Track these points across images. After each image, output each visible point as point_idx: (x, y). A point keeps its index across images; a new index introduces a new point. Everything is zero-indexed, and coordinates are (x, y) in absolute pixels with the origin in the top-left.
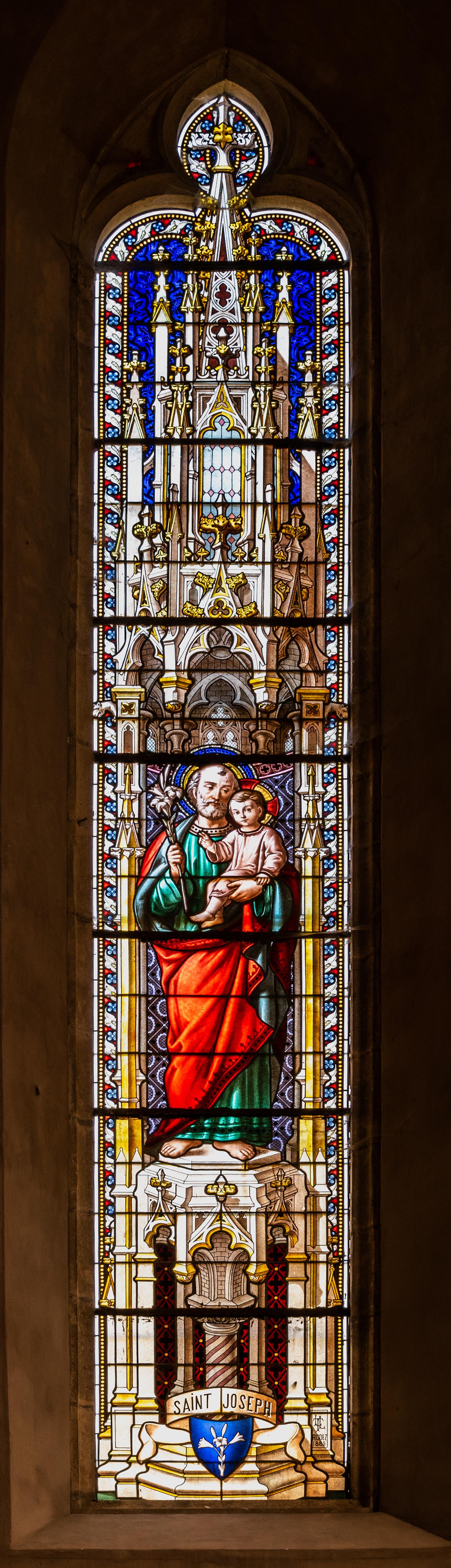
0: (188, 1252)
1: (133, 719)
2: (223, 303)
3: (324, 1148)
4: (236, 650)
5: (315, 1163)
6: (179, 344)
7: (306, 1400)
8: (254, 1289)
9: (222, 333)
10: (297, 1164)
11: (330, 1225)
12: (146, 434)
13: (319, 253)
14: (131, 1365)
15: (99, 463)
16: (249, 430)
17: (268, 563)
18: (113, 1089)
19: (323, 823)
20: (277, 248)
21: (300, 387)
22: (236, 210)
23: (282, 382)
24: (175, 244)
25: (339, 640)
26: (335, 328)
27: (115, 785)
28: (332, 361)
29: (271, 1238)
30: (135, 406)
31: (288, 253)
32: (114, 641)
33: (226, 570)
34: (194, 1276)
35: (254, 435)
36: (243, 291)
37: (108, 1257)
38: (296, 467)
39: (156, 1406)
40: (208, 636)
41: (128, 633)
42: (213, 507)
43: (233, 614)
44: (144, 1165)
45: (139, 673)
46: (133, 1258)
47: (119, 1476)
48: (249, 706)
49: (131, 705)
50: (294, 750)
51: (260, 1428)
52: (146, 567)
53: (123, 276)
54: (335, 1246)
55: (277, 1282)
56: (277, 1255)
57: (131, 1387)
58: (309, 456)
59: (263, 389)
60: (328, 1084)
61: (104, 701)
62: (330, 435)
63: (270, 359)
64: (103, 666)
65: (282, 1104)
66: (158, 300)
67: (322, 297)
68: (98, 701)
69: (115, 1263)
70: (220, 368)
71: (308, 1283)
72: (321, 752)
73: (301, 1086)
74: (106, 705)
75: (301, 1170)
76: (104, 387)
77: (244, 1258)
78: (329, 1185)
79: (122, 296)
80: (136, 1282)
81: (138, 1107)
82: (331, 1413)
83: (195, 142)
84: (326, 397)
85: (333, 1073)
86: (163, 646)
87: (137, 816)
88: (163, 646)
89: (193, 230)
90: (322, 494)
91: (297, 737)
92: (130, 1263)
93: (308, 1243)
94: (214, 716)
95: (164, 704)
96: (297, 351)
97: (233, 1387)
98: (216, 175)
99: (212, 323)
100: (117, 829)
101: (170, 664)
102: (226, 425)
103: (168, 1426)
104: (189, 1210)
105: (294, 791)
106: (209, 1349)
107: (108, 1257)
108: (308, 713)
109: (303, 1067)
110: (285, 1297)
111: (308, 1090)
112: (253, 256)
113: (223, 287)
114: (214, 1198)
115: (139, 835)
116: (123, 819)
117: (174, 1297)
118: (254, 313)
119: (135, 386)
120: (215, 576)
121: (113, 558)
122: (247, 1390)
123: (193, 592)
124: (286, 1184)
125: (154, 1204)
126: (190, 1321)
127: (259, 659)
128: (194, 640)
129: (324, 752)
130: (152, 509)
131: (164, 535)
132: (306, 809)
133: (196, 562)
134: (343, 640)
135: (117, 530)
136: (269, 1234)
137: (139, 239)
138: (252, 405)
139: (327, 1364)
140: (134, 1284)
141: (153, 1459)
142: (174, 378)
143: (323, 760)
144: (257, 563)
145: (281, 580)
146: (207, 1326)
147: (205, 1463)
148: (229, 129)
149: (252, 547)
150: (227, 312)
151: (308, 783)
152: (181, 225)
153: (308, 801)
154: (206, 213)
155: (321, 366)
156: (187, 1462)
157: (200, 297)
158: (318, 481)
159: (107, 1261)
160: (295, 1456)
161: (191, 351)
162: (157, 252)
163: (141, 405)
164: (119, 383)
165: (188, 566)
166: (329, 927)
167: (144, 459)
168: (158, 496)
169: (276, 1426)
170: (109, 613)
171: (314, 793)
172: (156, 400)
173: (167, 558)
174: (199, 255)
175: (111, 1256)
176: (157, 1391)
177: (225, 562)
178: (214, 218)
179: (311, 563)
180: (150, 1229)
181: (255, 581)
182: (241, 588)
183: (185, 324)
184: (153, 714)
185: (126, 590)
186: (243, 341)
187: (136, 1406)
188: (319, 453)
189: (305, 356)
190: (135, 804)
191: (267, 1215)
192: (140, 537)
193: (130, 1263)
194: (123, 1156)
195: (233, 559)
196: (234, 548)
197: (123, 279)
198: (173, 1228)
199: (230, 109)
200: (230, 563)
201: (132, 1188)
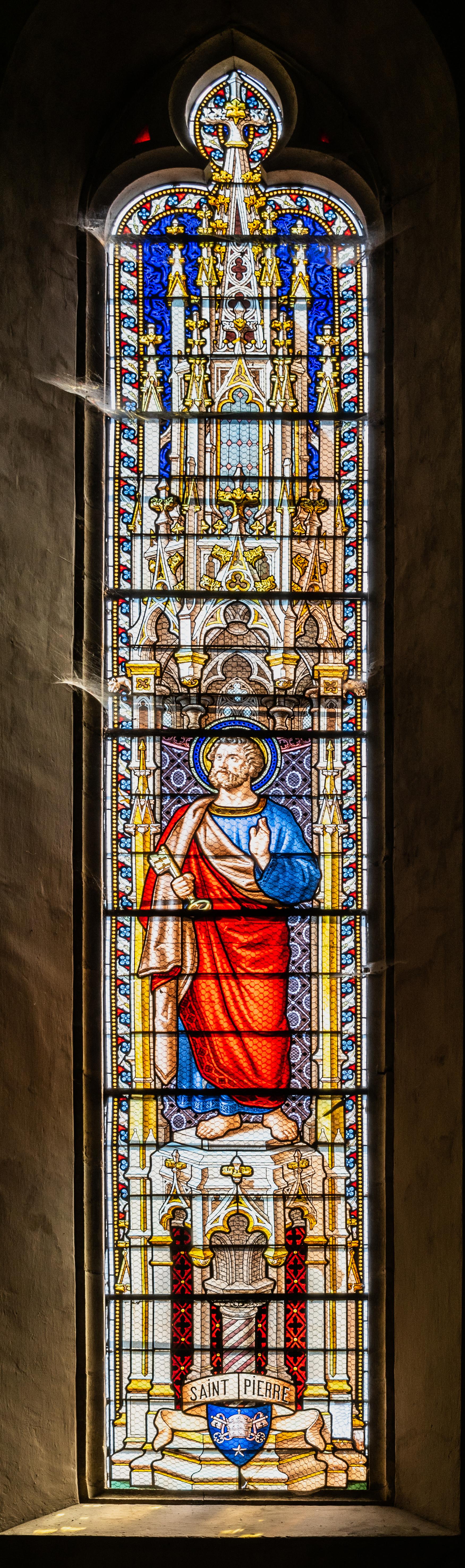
1: (148, 695)
3: (343, 1130)
6: (195, 318)
7: (326, 1387)
8: (272, 1273)
11: (348, 1207)
14: (147, 1351)
15: (116, 435)
16: (268, 403)
23: (300, 356)
24: (190, 218)
25: (357, 584)
27: (128, 761)
28: (350, 335)
29: (289, 1221)
31: (303, 226)
32: (128, 614)
33: (243, 543)
35: (273, 408)
37: (123, 1240)
38: (315, 442)
39: (172, 1392)
40: (225, 612)
41: (143, 607)
43: (250, 588)
48: (266, 682)
50: (312, 727)
51: (279, 1414)
53: (137, 249)
55: (296, 1267)
56: (296, 1241)
60: (346, 1065)
61: (118, 676)
62: (350, 408)
63: (288, 333)
68: (113, 676)
70: (237, 342)
71: (328, 1267)
72: (340, 729)
73: (318, 1066)
74: (121, 680)
75: (319, 1152)
76: (121, 360)
78: (348, 1168)
79: (137, 270)
80: (153, 1266)
81: (153, 1087)
84: (344, 371)
85: (351, 1055)
86: (179, 620)
87: (152, 793)
88: (179, 620)
89: (207, 204)
90: (341, 469)
94: (230, 692)
95: (179, 679)
96: (315, 330)
97: (251, 1373)
98: (229, 150)
101: (186, 640)
103: (185, 1412)
105: (311, 767)
106: (226, 1333)
107: (123, 1240)
109: (321, 1047)
110: (304, 1281)
111: (326, 1071)
112: (270, 230)
117: (191, 1282)
118: (271, 287)
122: (265, 1375)
123: (210, 565)
124: (304, 1165)
126: (208, 1305)
127: (276, 635)
128: (209, 617)
129: (342, 728)
131: (181, 508)
132: (326, 784)
134: (362, 553)
137: (153, 213)
138: (271, 378)
140: (149, 1267)
141: (171, 1446)
143: (342, 734)
145: (299, 554)
147: (222, 1452)
152: (195, 199)
153: (327, 777)
155: (340, 340)
156: (204, 1449)
164: (137, 357)
168: (175, 468)
169: (295, 1412)
170: (125, 586)
174: (213, 229)
175: (126, 1239)
176: (173, 1377)
177: (243, 537)
179: (330, 537)
188: (338, 427)
189: (323, 330)
190: (151, 779)
195: (251, 531)
197: (138, 252)
198: (189, 1210)
199: (242, 85)
201: (147, 1170)
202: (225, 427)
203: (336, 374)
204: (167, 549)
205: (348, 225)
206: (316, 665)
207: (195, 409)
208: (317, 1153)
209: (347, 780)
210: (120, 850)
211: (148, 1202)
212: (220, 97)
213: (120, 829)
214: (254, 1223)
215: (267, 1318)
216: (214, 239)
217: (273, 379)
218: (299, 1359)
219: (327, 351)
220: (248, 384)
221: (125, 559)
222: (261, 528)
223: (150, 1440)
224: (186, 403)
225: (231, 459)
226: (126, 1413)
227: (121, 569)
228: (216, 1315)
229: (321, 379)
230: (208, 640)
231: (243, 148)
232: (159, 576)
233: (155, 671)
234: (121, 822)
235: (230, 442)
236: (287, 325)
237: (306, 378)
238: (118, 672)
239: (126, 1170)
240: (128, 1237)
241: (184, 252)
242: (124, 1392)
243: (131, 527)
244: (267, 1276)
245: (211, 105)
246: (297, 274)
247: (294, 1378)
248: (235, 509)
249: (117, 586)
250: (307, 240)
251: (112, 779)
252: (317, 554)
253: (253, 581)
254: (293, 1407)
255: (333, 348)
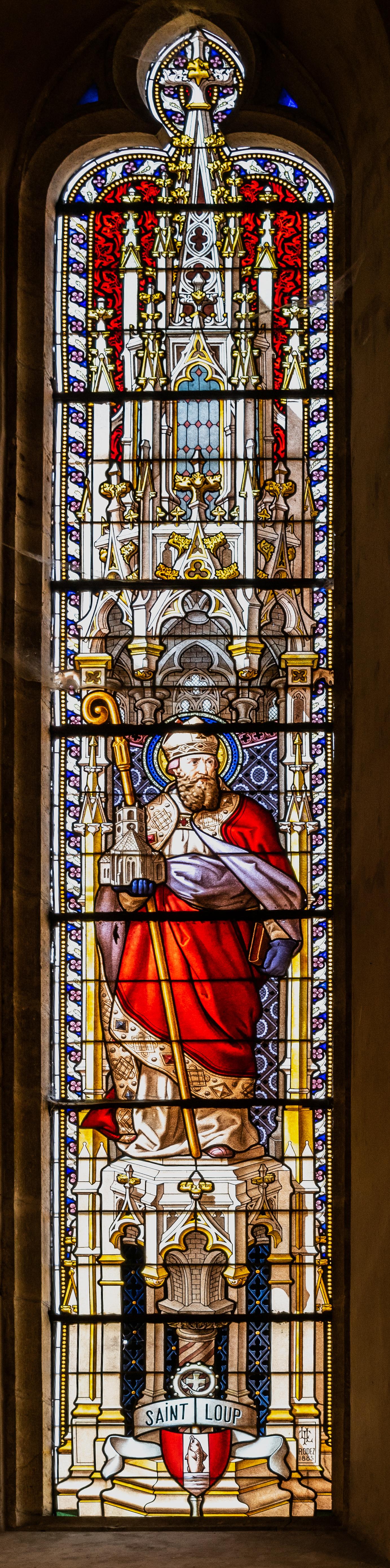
0: (159, 1254)
2: (199, 248)
4: (214, 615)
5: (301, 1158)
6: (150, 291)
7: (291, 1413)
8: (233, 1294)
9: (198, 279)
10: (281, 1159)
11: (317, 1224)
12: (116, 387)
13: (305, 194)
15: (63, 419)
16: (229, 380)
17: (250, 521)
18: (77, 1081)
19: (311, 796)
20: (261, 189)
21: (284, 333)
22: (215, 152)
23: (264, 329)
26: (325, 274)
27: (78, 758)
29: (251, 1238)
30: (102, 356)
31: (272, 193)
32: (78, 607)
33: (203, 530)
34: (166, 1279)
35: (235, 386)
36: (222, 234)
37: (69, 1258)
38: (281, 420)
39: (122, 1417)
42: (189, 465)
43: (211, 576)
44: (110, 1161)
45: (106, 641)
46: (97, 1260)
47: (81, 1494)
49: (97, 673)
50: (278, 719)
52: (115, 528)
54: (324, 1248)
55: (258, 1286)
56: (258, 1257)
57: (94, 1397)
58: (295, 406)
59: (243, 336)
60: (316, 1075)
61: (66, 670)
64: (66, 633)
65: (266, 1092)
66: (126, 244)
67: (309, 241)
69: (77, 1265)
70: (195, 315)
72: (308, 720)
73: (285, 1076)
77: (222, 1259)
78: (316, 1181)
79: (86, 242)
80: (101, 1286)
82: (320, 1425)
83: (168, 77)
85: (322, 1063)
87: (103, 790)
91: (282, 705)
92: (94, 1265)
93: (294, 1243)
95: (133, 672)
96: (281, 297)
98: (190, 113)
99: (187, 269)
100: (81, 804)
101: (140, 630)
102: (204, 375)
103: (136, 1438)
104: (160, 1208)
108: (294, 679)
109: (289, 1056)
110: (268, 1302)
111: (294, 1083)
112: (234, 197)
113: (199, 230)
114: (187, 1195)
115: (105, 810)
116: (87, 793)
117: (143, 1302)
119: (101, 336)
120: (191, 536)
121: (79, 519)
122: (224, 1399)
125: (121, 1202)
127: (239, 624)
128: (168, 605)
129: (311, 719)
130: (121, 467)
131: (135, 495)
132: (292, 780)
133: (171, 521)
135: (81, 490)
136: (250, 1235)
138: (232, 353)
139: (315, 1373)
140: (98, 1288)
141: (120, 1475)
142: (144, 326)
144: (238, 523)
146: (180, 1332)
148: (206, 64)
149: (233, 504)
150: (203, 257)
151: (295, 753)
153: (294, 772)
154: (180, 154)
155: (309, 313)
156: (158, 1478)
157: (173, 242)
158: (306, 437)
159: (67, 1263)
160: (280, 1472)
161: (164, 297)
162: (128, 194)
163: (108, 355)
164: (85, 333)
165: (162, 526)
166: (318, 905)
167: (112, 414)
168: (128, 452)
169: (257, 1437)
170: (73, 577)
171: (301, 763)
172: (126, 350)
173: (138, 519)
175: (73, 1258)
177: (203, 521)
178: (190, 158)
180: (116, 1229)
181: (236, 541)
182: (221, 551)
183: (157, 270)
184: (119, 676)
185: (94, 540)
186: (221, 287)
187: (100, 1418)
189: (290, 301)
191: (248, 1213)
192: (108, 496)
193: (94, 1265)
194: (83, 1153)
195: (212, 518)
196: (212, 506)
198: (141, 1227)
199: (206, 44)
200: (207, 522)
201: (97, 1184)
202: (182, 405)
203: (303, 348)
204: (119, 539)
205: (321, 190)
206: (284, 653)
207: (149, 388)
208: (284, 1168)
209: (316, 774)
210: (69, 850)
211: (98, 1217)
212: (180, 58)
213: (69, 827)
214: (212, 1241)
215: (227, 1341)
216: (175, 207)
217: (235, 355)
218: (261, 1383)
219: (294, 324)
220: (206, 362)
221: (73, 549)
222: (223, 513)
223: (99, 1468)
224: (140, 382)
225: (192, 438)
226: (72, 1439)
227: (69, 560)
228: (172, 1338)
229: (288, 353)
230: (164, 630)
231: (206, 110)
232: (111, 566)
233: (107, 664)
234: (70, 820)
235: (187, 425)
236: (250, 296)
237: (270, 353)
238: (65, 666)
239: (75, 1184)
240: (75, 1256)
241: (140, 222)
242: (70, 1417)
243: (80, 515)
244: (226, 1297)
245: (171, 66)
246: (262, 244)
247: (257, 1402)
248: (195, 494)
249: (64, 578)
250: (273, 207)
251: (61, 1417)
252: (283, 538)
253: (214, 569)
254: (255, 1432)
255: (301, 321)
